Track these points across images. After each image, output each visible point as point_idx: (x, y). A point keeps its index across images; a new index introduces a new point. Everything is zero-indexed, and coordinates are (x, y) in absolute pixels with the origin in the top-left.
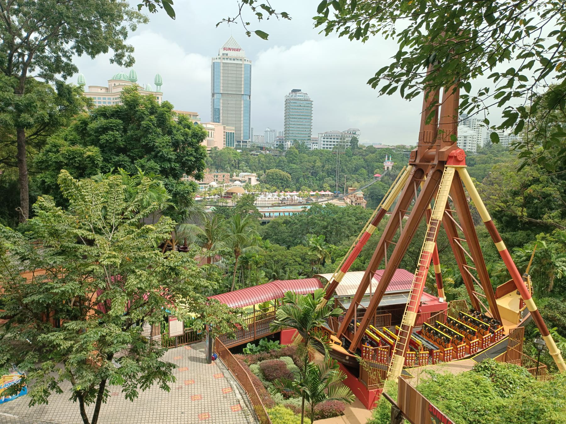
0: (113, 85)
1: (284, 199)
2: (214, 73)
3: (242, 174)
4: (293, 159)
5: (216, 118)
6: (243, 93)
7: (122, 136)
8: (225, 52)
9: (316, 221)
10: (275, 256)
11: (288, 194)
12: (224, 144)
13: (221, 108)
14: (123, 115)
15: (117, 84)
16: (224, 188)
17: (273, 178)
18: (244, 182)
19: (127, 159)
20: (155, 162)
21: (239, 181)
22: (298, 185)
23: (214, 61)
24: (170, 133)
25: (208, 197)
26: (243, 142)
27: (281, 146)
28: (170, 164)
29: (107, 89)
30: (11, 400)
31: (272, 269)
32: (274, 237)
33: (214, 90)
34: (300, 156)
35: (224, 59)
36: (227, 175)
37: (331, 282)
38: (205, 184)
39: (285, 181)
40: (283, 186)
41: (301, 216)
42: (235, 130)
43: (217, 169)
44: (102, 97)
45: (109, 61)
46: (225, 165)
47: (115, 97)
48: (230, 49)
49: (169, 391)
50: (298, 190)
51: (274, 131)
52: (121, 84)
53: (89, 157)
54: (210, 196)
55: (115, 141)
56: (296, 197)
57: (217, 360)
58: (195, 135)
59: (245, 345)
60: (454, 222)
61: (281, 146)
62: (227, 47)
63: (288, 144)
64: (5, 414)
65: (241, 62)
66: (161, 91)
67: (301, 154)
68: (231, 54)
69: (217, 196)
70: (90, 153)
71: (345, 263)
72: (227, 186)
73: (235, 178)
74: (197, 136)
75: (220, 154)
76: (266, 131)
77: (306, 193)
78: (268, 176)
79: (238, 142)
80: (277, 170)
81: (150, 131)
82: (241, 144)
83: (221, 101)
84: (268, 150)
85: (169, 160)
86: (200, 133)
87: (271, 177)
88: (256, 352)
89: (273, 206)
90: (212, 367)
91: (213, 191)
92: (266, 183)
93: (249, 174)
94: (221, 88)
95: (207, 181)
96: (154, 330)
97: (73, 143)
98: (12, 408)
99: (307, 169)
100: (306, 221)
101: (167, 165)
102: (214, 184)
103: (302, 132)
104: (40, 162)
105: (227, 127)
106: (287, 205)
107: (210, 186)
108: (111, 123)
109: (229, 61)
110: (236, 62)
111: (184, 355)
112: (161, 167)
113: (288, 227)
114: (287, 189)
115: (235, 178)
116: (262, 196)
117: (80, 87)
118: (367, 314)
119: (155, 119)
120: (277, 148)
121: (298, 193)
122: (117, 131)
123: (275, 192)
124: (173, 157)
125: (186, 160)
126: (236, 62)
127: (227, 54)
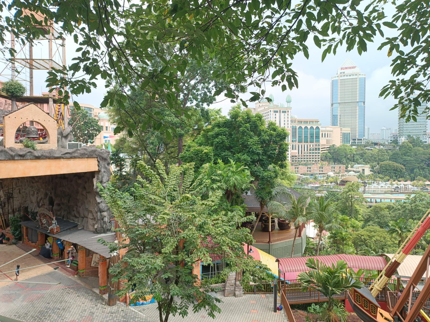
1: (398, 187)
2: (333, 88)
3: (357, 166)
4: (407, 152)
5: (334, 121)
6: (358, 101)
7: (228, 139)
8: (343, 71)
9: (420, 208)
10: (374, 236)
11: (401, 183)
12: (341, 142)
13: (339, 115)
14: (229, 125)
16: (340, 177)
17: (386, 169)
18: (358, 172)
19: (230, 153)
20: (248, 155)
21: (354, 171)
22: (412, 175)
23: (333, 79)
24: (259, 135)
25: (325, 184)
26: (358, 140)
27: (395, 142)
28: (259, 156)
30: (146, 304)
31: (371, 248)
32: (377, 220)
33: (333, 101)
34: (415, 150)
35: (341, 76)
36: (343, 167)
37: (393, 261)
38: (324, 174)
39: (398, 172)
40: (396, 176)
41: (405, 203)
42: (351, 131)
43: (335, 162)
46: (341, 159)
48: (346, 68)
49: (214, 318)
50: (412, 179)
51: (390, 129)
52: (263, 104)
53: (205, 153)
54: (327, 183)
55: (223, 142)
56: (410, 186)
57: (282, 311)
58: (279, 135)
59: (310, 305)
61: (395, 142)
62: (344, 67)
63: (403, 140)
64: (139, 313)
65: (356, 77)
67: (416, 148)
68: (347, 71)
69: (333, 184)
70: (206, 151)
71: (407, 245)
72: (343, 176)
73: (349, 169)
74: (280, 136)
75: (338, 151)
76: (382, 130)
77: (421, 182)
78: (381, 167)
79: (353, 140)
80: (390, 162)
81: (245, 134)
82: (357, 141)
83: (339, 109)
84: (382, 145)
85: (258, 154)
86: (282, 133)
87: (384, 168)
88: (319, 313)
89: (385, 193)
90: (277, 315)
91: (330, 179)
92: (379, 173)
93: (363, 165)
94: (339, 99)
95: (326, 171)
96: (237, 277)
97: (200, 145)
98: (144, 310)
99: (423, 161)
100: (409, 208)
101: (256, 157)
102: (331, 174)
104: (182, 157)
105: (343, 129)
106: (401, 193)
107: (328, 175)
108: (221, 131)
110: (352, 77)
111: (258, 301)
112: (251, 159)
113: (390, 212)
114: (401, 179)
115: (349, 169)
116: (375, 185)
117: (219, 110)
118: (420, 297)
119: (249, 126)
120: (391, 143)
121: (412, 183)
122: (224, 135)
123: (388, 181)
124: (260, 152)
125: (271, 153)
126: (352, 77)
127: (344, 73)
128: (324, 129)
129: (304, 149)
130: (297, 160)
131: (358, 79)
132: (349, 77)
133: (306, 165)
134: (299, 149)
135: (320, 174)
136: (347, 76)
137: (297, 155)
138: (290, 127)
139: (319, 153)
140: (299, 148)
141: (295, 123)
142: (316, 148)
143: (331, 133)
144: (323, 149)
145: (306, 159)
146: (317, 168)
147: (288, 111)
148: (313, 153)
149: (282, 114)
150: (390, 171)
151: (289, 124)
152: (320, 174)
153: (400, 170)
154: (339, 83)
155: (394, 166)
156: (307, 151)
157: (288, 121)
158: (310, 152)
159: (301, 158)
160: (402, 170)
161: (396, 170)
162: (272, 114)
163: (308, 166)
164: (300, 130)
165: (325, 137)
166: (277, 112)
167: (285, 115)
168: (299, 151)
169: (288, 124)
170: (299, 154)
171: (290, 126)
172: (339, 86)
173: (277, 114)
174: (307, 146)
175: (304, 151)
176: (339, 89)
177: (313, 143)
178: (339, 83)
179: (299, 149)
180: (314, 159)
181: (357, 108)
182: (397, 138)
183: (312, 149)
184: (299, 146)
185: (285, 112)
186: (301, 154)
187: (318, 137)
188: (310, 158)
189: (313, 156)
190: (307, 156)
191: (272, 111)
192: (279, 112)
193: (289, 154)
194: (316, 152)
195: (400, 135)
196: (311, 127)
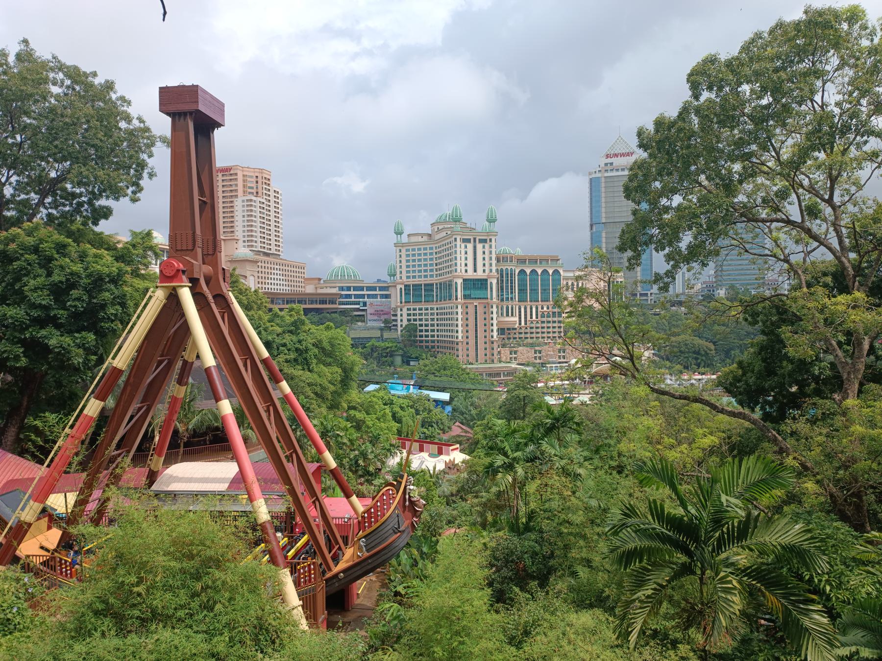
0: (436, 230)
8: (609, 160)
15: (440, 227)
17: (681, 352)
26: (641, 295)
29: (430, 235)
35: (606, 171)
39: (702, 356)
44: (422, 247)
45: (154, 178)
47: (437, 245)
48: (616, 155)
52: (446, 226)
60: (186, 330)
66: (496, 230)
94: (604, 215)
103: (748, 272)
109: (614, 173)
127: (611, 164)
129: (531, 315)
130: (517, 336)
133: (532, 345)
134: (520, 315)
135: (560, 363)
136: (617, 170)
137: (517, 326)
138: (494, 271)
140: (520, 312)
141: (505, 263)
142: (554, 313)
145: (534, 335)
146: (554, 351)
147: (491, 240)
149: (479, 246)
150: (687, 355)
151: (494, 265)
152: (560, 363)
153: (706, 352)
154: (603, 185)
155: (693, 344)
156: (537, 317)
157: (491, 259)
159: (526, 333)
160: (708, 352)
161: (698, 353)
162: (458, 246)
163: (537, 348)
164: (522, 276)
166: (468, 241)
168: (520, 318)
169: (491, 265)
170: (520, 324)
171: (494, 268)
172: (603, 190)
174: (537, 308)
175: (531, 318)
176: (603, 195)
178: (603, 185)
179: (520, 315)
180: (551, 335)
182: (713, 291)
183: (546, 313)
184: (520, 309)
185: (485, 241)
186: (526, 324)
188: (543, 333)
189: (548, 327)
190: (537, 328)
191: (458, 240)
192: (472, 241)
193: (495, 325)
195: (719, 286)
196: (554, 272)
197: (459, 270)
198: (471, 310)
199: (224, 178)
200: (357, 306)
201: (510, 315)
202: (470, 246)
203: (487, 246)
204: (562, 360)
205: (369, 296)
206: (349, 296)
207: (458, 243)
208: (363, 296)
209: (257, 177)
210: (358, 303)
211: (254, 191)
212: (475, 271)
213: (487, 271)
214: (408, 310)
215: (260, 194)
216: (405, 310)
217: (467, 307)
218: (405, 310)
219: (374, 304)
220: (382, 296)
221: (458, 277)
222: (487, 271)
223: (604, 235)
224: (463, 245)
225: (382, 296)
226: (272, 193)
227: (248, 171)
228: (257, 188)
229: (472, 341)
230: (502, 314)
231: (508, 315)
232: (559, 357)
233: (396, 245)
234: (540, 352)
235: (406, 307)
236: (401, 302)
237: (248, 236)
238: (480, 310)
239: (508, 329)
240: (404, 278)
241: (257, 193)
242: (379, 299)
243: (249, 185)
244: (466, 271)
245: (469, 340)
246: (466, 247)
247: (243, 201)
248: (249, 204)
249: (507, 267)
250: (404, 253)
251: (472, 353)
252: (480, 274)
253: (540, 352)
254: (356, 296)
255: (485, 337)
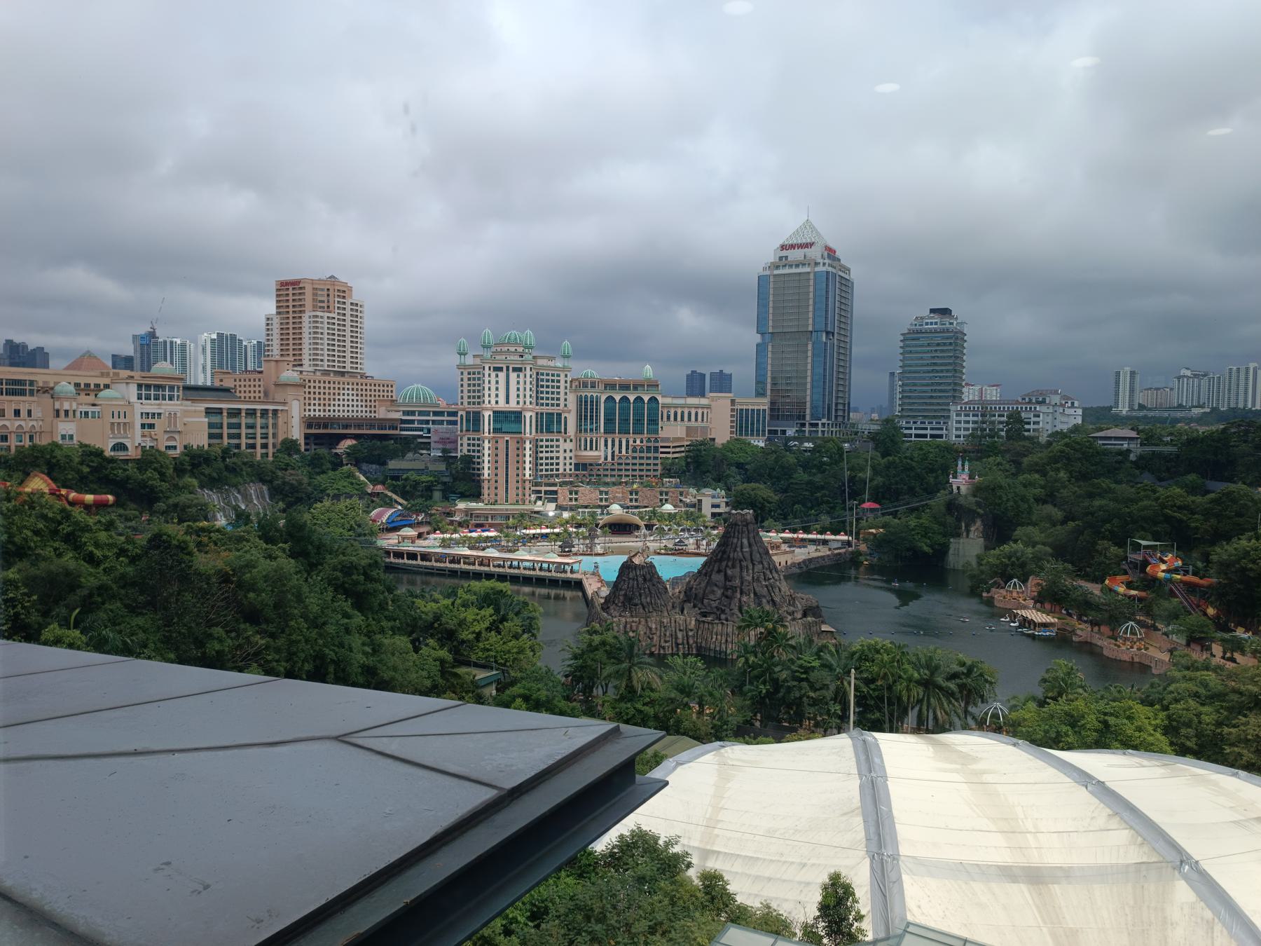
8: (785, 253)
65: (807, 269)
76: (1179, 378)
127: (786, 257)
128: (668, 401)
131: (812, 276)
132: (794, 270)
136: (791, 266)
139: (656, 458)
141: (593, 390)
143: (705, 411)
144: (678, 450)
148: (641, 458)
149: (513, 376)
158: (635, 455)
165: (682, 419)
166: (500, 369)
167: (518, 376)
173: (500, 374)
174: (628, 442)
175: (620, 452)
177: (641, 436)
181: (810, 347)
183: (638, 448)
185: (520, 370)
186: (613, 459)
187: (653, 421)
192: (505, 369)
194: (649, 455)
196: (650, 399)
197: (487, 402)
198: (502, 445)
199: (295, 292)
200: (421, 433)
201: (594, 448)
202: (502, 375)
203: (522, 375)
204: (634, 503)
205: (434, 422)
206: (412, 422)
207: (487, 372)
208: (427, 422)
209: (328, 290)
210: (421, 430)
211: (325, 305)
212: (508, 402)
213: (521, 403)
214: (469, 439)
215: (331, 308)
216: (465, 439)
217: (497, 442)
218: (465, 439)
219: (438, 431)
220: (450, 423)
221: (487, 409)
222: (521, 403)
223: (770, 348)
224: (493, 374)
225: (450, 423)
226: (348, 307)
227: (319, 284)
228: (328, 302)
229: (502, 480)
230: (580, 449)
231: (586, 449)
232: (631, 500)
233: (459, 367)
234: (576, 493)
235: (467, 437)
236: (461, 431)
237: (314, 354)
238: (512, 446)
239: (591, 465)
240: (465, 404)
241: (328, 307)
242: (445, 426)
243: (320, 298)
244: (497, 402)
245: (498, 478)
246: (497, 376)
247: (310, 317)
248: (315, 320)
249: (589, 393)
250: (466, 376)
251: (502, 492)
252: (513, 406)
253: (607, 493)
254: (421, 422)
255: (518, 475)
